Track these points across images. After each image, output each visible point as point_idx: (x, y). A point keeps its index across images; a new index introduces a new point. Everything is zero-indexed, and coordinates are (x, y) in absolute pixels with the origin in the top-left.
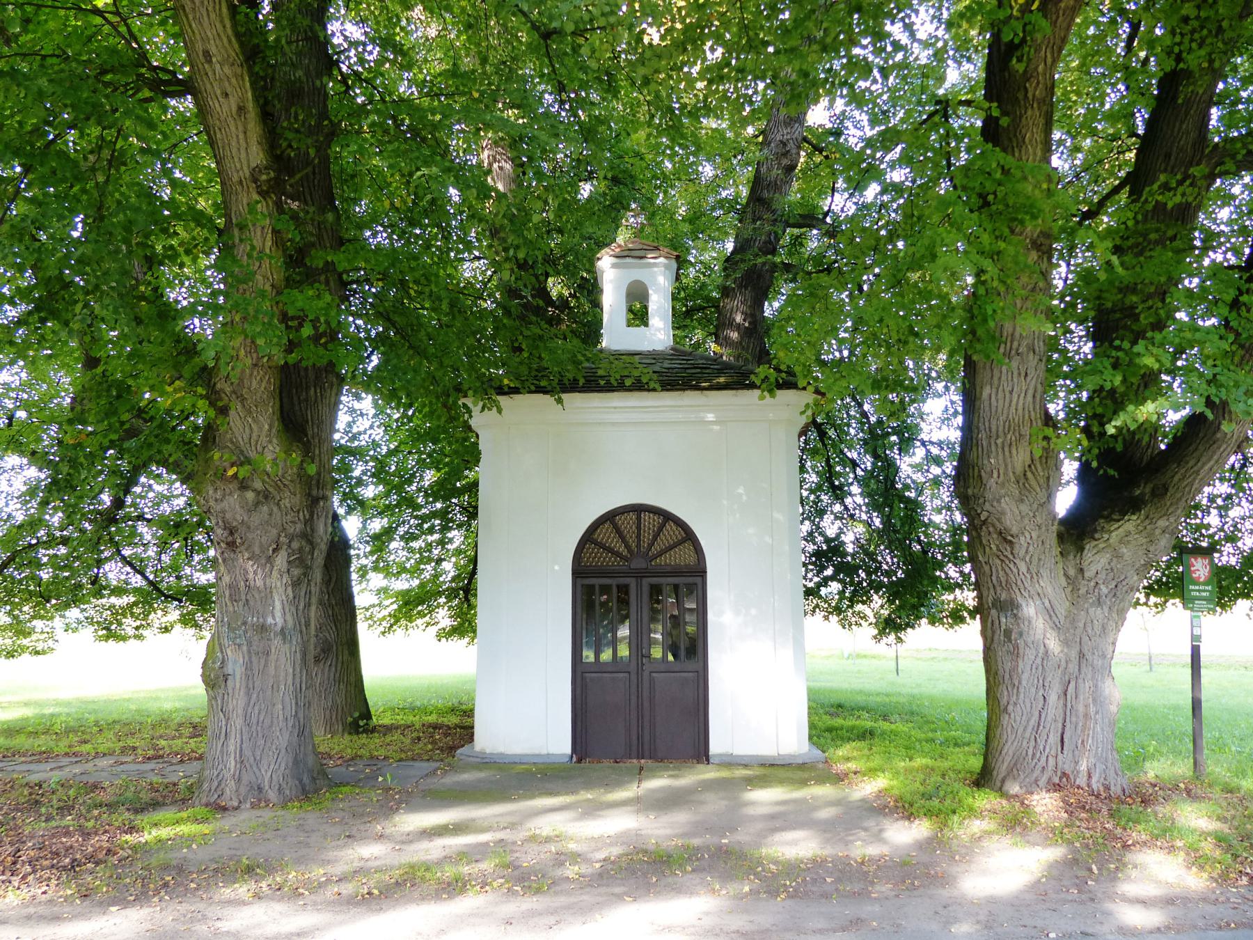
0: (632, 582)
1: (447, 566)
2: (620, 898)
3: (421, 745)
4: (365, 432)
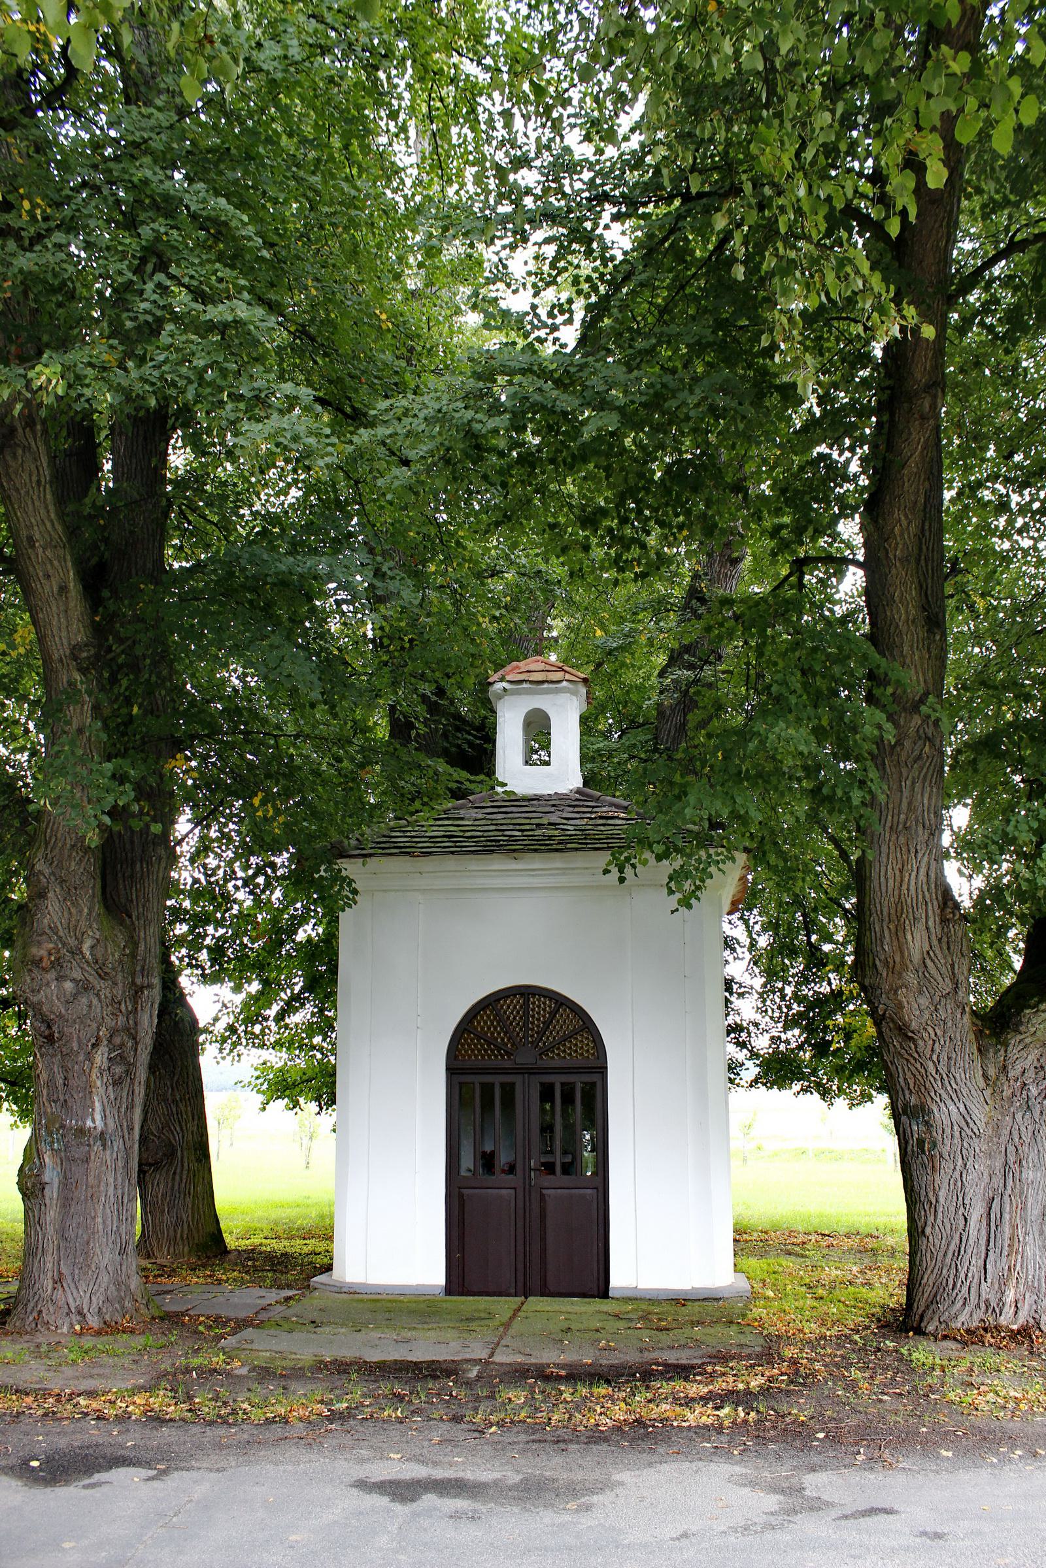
0: (517, 1080)
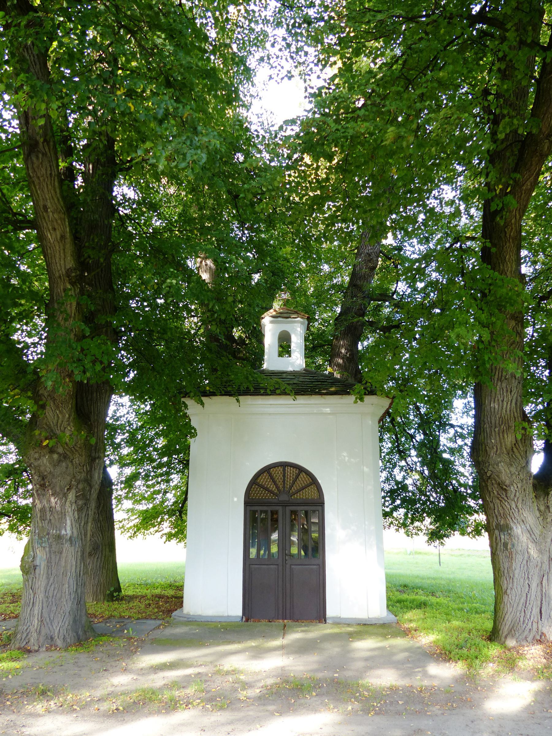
0: (280, 509)
1: (169, 496)
2: (272, 714)
3: (151, 609)
4: (124, 416)
